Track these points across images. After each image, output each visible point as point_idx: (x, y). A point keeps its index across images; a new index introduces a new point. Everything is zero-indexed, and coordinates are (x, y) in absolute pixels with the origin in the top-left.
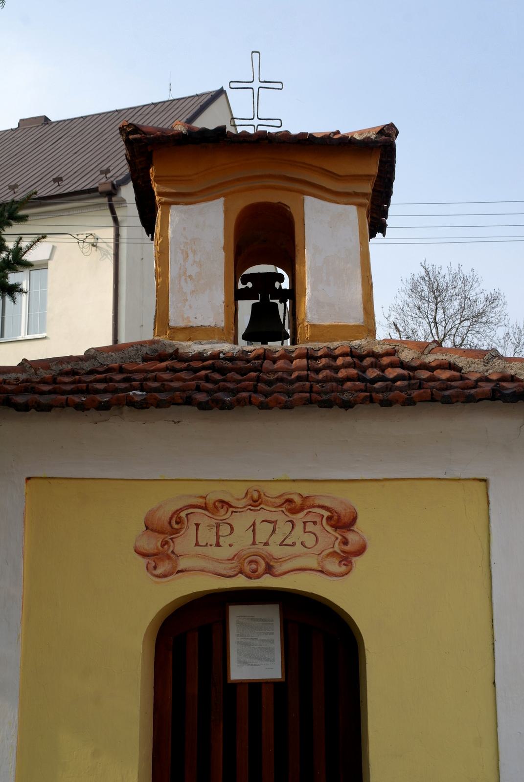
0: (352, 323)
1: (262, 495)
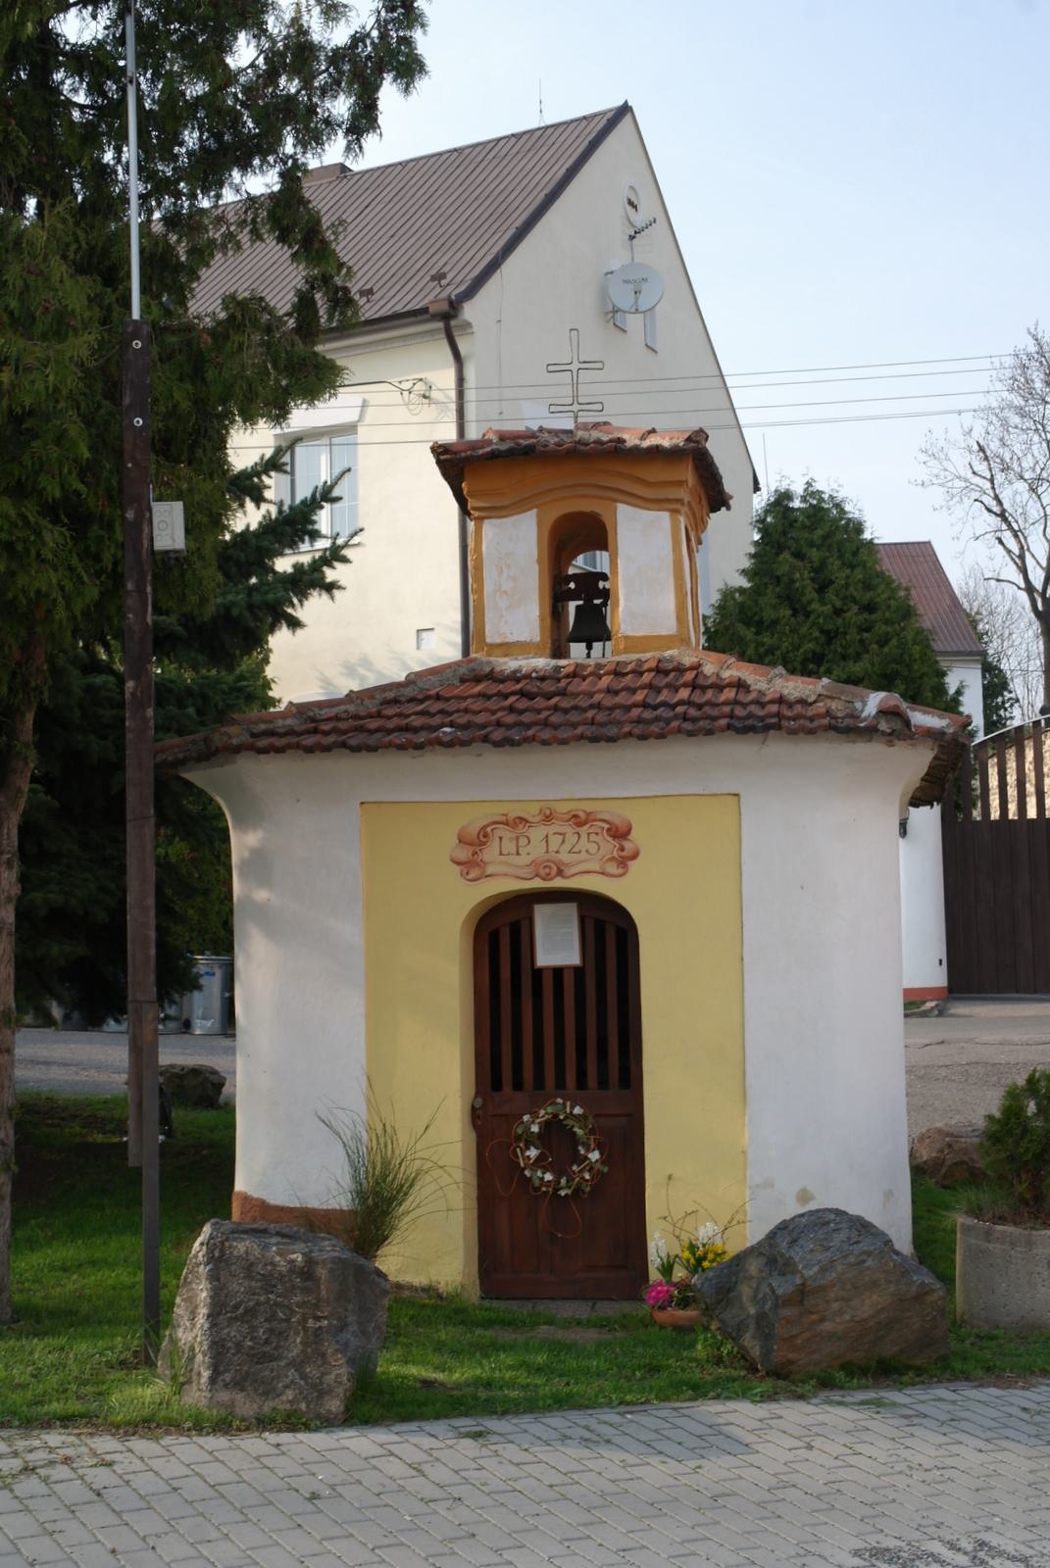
0: (664, 632)
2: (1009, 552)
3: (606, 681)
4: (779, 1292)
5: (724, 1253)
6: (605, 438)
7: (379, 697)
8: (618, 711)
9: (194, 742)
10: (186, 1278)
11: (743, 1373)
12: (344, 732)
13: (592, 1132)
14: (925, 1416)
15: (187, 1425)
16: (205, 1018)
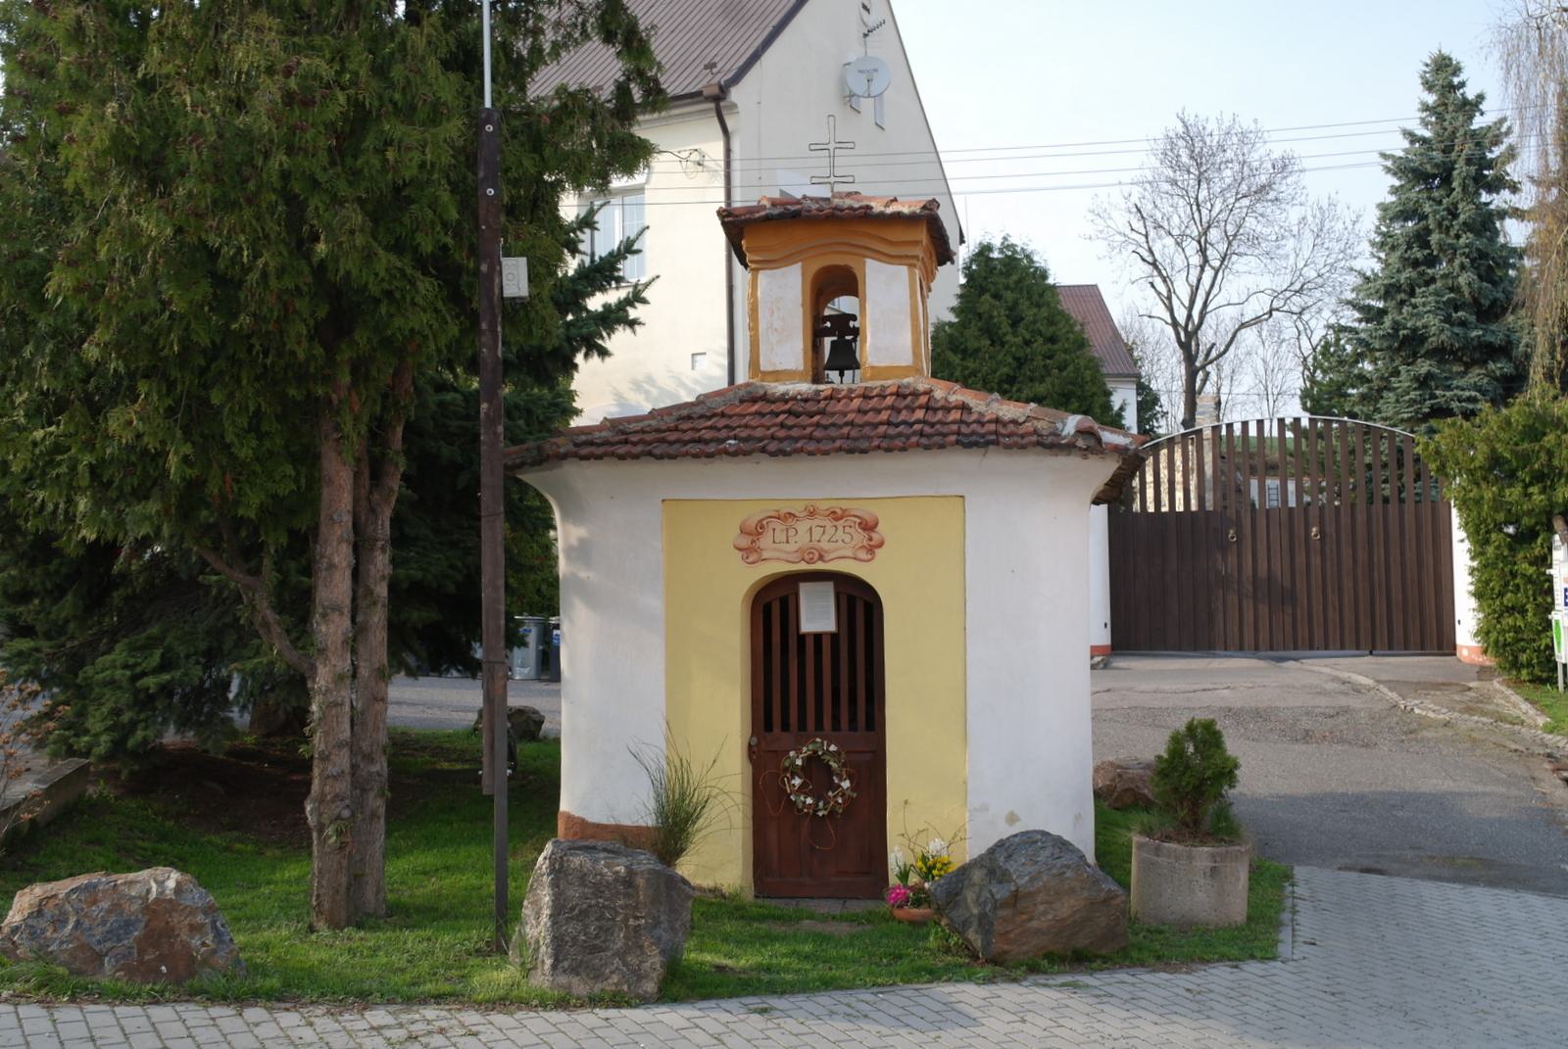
2: (1159, 293)
3: (856, 403)
4: (998, 897)
5: (949, 863)
6: (856, 206)
7: (676, 414)
8: (867, 428)
9: (528, 450)
10: (532, 886)
11: (967, 961)
12: (650, 443)
13: (844, 765)
14: (1112, 996)
15: (534, 1003)
16: (523, 666)
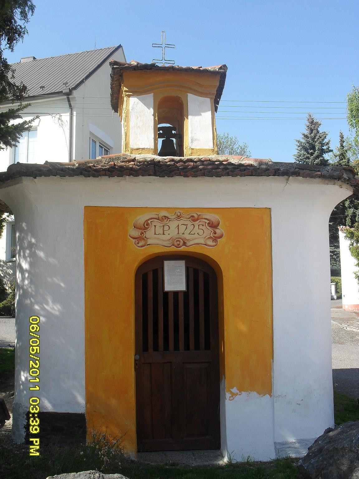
1: (182, 214)
